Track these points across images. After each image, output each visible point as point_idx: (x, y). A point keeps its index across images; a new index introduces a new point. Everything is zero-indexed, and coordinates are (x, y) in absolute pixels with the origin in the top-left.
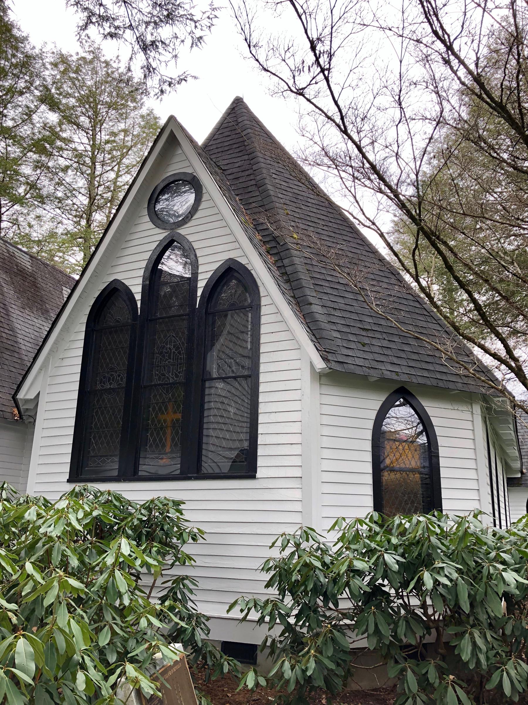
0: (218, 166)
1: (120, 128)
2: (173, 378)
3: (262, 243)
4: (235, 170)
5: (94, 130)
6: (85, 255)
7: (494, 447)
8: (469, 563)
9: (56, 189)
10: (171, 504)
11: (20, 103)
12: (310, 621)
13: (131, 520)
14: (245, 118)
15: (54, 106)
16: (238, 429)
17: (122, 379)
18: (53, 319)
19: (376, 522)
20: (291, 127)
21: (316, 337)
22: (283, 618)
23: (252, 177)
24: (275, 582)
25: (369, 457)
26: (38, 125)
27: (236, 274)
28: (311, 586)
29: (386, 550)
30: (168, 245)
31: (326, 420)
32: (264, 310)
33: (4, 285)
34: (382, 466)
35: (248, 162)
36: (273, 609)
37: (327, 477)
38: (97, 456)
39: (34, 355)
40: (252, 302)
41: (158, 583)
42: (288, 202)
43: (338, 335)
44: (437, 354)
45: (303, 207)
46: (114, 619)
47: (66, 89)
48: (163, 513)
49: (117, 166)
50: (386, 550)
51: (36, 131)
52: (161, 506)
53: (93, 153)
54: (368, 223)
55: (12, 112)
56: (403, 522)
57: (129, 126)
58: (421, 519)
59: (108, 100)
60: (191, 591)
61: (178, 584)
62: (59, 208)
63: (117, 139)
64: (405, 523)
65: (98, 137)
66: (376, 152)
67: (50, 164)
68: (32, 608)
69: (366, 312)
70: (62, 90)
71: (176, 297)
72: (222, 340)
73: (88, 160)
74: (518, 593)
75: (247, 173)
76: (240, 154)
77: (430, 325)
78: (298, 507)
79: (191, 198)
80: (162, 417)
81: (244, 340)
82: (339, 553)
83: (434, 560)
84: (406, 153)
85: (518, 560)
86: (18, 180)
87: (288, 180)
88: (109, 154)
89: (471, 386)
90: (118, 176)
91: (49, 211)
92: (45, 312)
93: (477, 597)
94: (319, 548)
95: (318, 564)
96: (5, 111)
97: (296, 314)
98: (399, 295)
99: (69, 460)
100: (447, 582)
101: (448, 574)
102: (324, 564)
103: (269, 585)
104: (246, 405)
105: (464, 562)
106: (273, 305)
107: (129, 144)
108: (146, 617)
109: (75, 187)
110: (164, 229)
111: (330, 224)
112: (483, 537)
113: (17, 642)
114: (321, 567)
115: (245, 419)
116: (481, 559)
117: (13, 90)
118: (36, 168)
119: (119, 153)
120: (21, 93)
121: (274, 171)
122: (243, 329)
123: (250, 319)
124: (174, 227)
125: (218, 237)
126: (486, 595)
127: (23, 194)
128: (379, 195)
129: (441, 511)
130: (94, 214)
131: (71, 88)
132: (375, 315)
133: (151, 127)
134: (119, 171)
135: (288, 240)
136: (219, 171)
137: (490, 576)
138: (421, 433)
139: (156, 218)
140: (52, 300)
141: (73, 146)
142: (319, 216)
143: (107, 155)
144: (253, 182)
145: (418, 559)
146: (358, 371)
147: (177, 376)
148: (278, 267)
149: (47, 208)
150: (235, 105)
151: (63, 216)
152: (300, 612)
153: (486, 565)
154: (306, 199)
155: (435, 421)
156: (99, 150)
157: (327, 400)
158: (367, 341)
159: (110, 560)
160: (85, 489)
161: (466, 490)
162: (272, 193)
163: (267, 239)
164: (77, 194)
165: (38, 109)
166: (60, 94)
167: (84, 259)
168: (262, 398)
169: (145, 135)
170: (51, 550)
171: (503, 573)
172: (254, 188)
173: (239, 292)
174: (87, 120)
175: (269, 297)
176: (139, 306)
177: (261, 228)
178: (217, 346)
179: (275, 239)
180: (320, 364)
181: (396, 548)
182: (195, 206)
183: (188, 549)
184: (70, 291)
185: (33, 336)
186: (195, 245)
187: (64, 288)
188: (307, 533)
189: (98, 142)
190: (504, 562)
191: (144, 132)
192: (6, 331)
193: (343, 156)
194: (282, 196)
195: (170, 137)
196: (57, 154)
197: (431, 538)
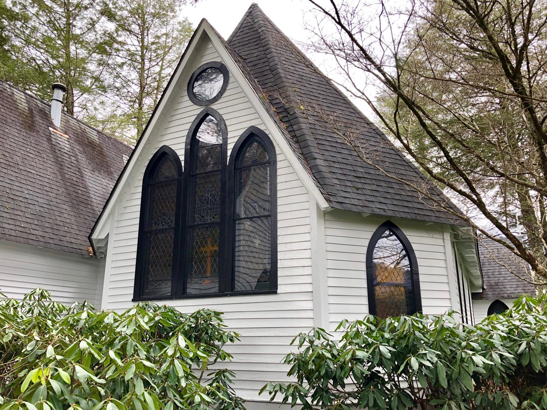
0: (240, 56)
1: (162, 33)
2: (211, 219)
3: (276, 114)
4: (253, 59)
5: (142, 34)
6: (138, 131)
7: (461, 268)
8: (446, 350)
9: (115, 81)
10: (213, 314)
11: (86, 16)
12: (323, 399)
13: (183, 327)
14: (260, 19)
15: (111, 17)
16: (262, 256)
17: (171, 221)
18: (117, 179)
19: (371, 323)
20: (297, 22)
21: (320, 184)
22: (303, 397)
23: (267, 64)
24: (295, 370)
25: (364, 275)
26: (100, 33)
27: (257, 138)
28: (323, 372)
29: (381, 343)
30: (202, 119)
31: (330, 247)
32: (279, 165)
33: (78, 154)
34: (375, 283)
35: (263, 52)
36: (294, 391)
37: (332, 291)
38: (154, 281)
39: (103, 207)
40: (269, 158)
41: (205, 376)
42: (295, 82)
43: (337, 182)
44: (415, 194)
45: (307, 85)
46: (175, 396)
47: (120, 4)
48: (207, 321)
49: (161, 62)
50: (381, 343)
51: (98, 37)
52: (206, 316)
53: (142, 53)
54: (359, 94)
55: (80, 23)
56: (393, 321)
57: (169, 31)
58: (407, 318)
59: (153, 11)
60: (230, 381)
61: (220, 375)
62: (118, 95)
63: (160, 41)
64: (394, 322)
65: (146, 40)
66: (363, 39)
67: (110, 62)
68: (113, 388)
69: (359, 164)
70: (117, 5)
71: (211, 157)
72: (247, 189)
73: (139, 58)
74: (485, 372)
75: (263, 61)
76: (257, 47)
77: (409, 173)
78: (310, 314)
79: (221, 78)
80: (203, 250)
81: (264, 188)
82: (345, 346)
83: (418, 349)
84: (387, 39)
85: (484, 348)
86: (85, 75)
87: (294, 65)
88: (155, 52)
89: (442, 219)
90: (162, 69)
91: (110, 97)
92: (110, 174)
93: (453, 376)
94: (328, 344)
95: (328, 355)
96: (74, 23)
97: (304, 167)
98: (384, 150)
99: (132, 284)
100: (430, 365)
101: (430, 359)
102: (333, 355)
103: (290, 374)
104: (267, 238)
105: (441, 350)
106: (286, 161)
107: (170, 45)
108: (199, 395)
109: (130, 79)
110: (201, 106)
111: (329, 98)
112: (456, 331)
113: (106, 406)
114: (331, 357)
115: (267, 249)
116: (455, 348)
117: (80, 6)
118: (100, 64)
119: (162, 52)
120: (86, 8)
121: (283, 59)
122: (262, 179)
123: (268, 173)
124: (208, 103)
125: (242, 111)
126: (459, 374)
127: (90, 86)
128: (367, 73)
129: (422, 313)
130: (144, 99)
131: (124, 3)
132: (366, 166)
133: (186, 31)
134: (162, 65)
135: (297, 111)
136: (241, 60)
137: (462, 360)
138: (404, 256)
139: (194, 98)
140: (115, 165)
141: (126, 47)
142: (319, 92)
143: (153, 54)
144: (268, 68)
145: (405, 348)
146: (354, 209)
147: (214, 218)
148: (289, 131)
149: (109, 95)
150: (251, 9)
151: (121, 101)
152: (315, 393)
153: (458, 352)
154: (309, 79)
155: (414, 247)
156: (147, 49)
157: (330, 232)
158: (360, 186)
159: (170, 352)
160: (146, 305)
161: (440, 300)
162: (282, 75)
163: (280, 110)
164: (131, 84)
165: (99, 19)
166: (116, 8)
167: (138, 133)
168: (279, 232)
169: (182, 37)
170: (127, 344)
171: (473, 357)
172: (268, 72)
173: (260, 151)
174: (137, 28)
175: (283, 155)
176: (183, 165)
177: (275, 102)
178: (244, 193)
179: (286, 110)
180: (324, 204)
181: (388, 341)
182: (224, 87)
183: (227, 349)
184: (128, 158)
185: (101, 192)
186: (225, 117)
187: (124, 156)
188: (319, 333)
189: (146, 44)
190: (473, 349)
191: (181, 35)
192: (81, 189)
193: (337, 45)
194: (290, 77)
195: (203, 36)
196: (115, 54)
197: (416, 332)
